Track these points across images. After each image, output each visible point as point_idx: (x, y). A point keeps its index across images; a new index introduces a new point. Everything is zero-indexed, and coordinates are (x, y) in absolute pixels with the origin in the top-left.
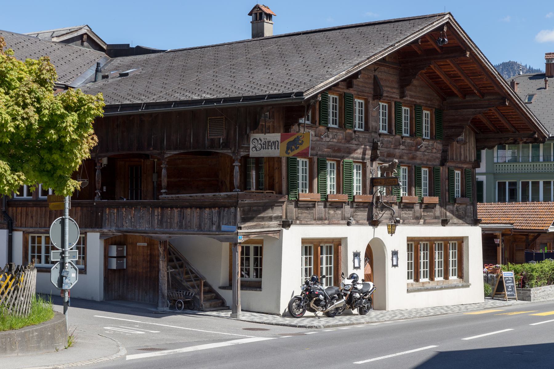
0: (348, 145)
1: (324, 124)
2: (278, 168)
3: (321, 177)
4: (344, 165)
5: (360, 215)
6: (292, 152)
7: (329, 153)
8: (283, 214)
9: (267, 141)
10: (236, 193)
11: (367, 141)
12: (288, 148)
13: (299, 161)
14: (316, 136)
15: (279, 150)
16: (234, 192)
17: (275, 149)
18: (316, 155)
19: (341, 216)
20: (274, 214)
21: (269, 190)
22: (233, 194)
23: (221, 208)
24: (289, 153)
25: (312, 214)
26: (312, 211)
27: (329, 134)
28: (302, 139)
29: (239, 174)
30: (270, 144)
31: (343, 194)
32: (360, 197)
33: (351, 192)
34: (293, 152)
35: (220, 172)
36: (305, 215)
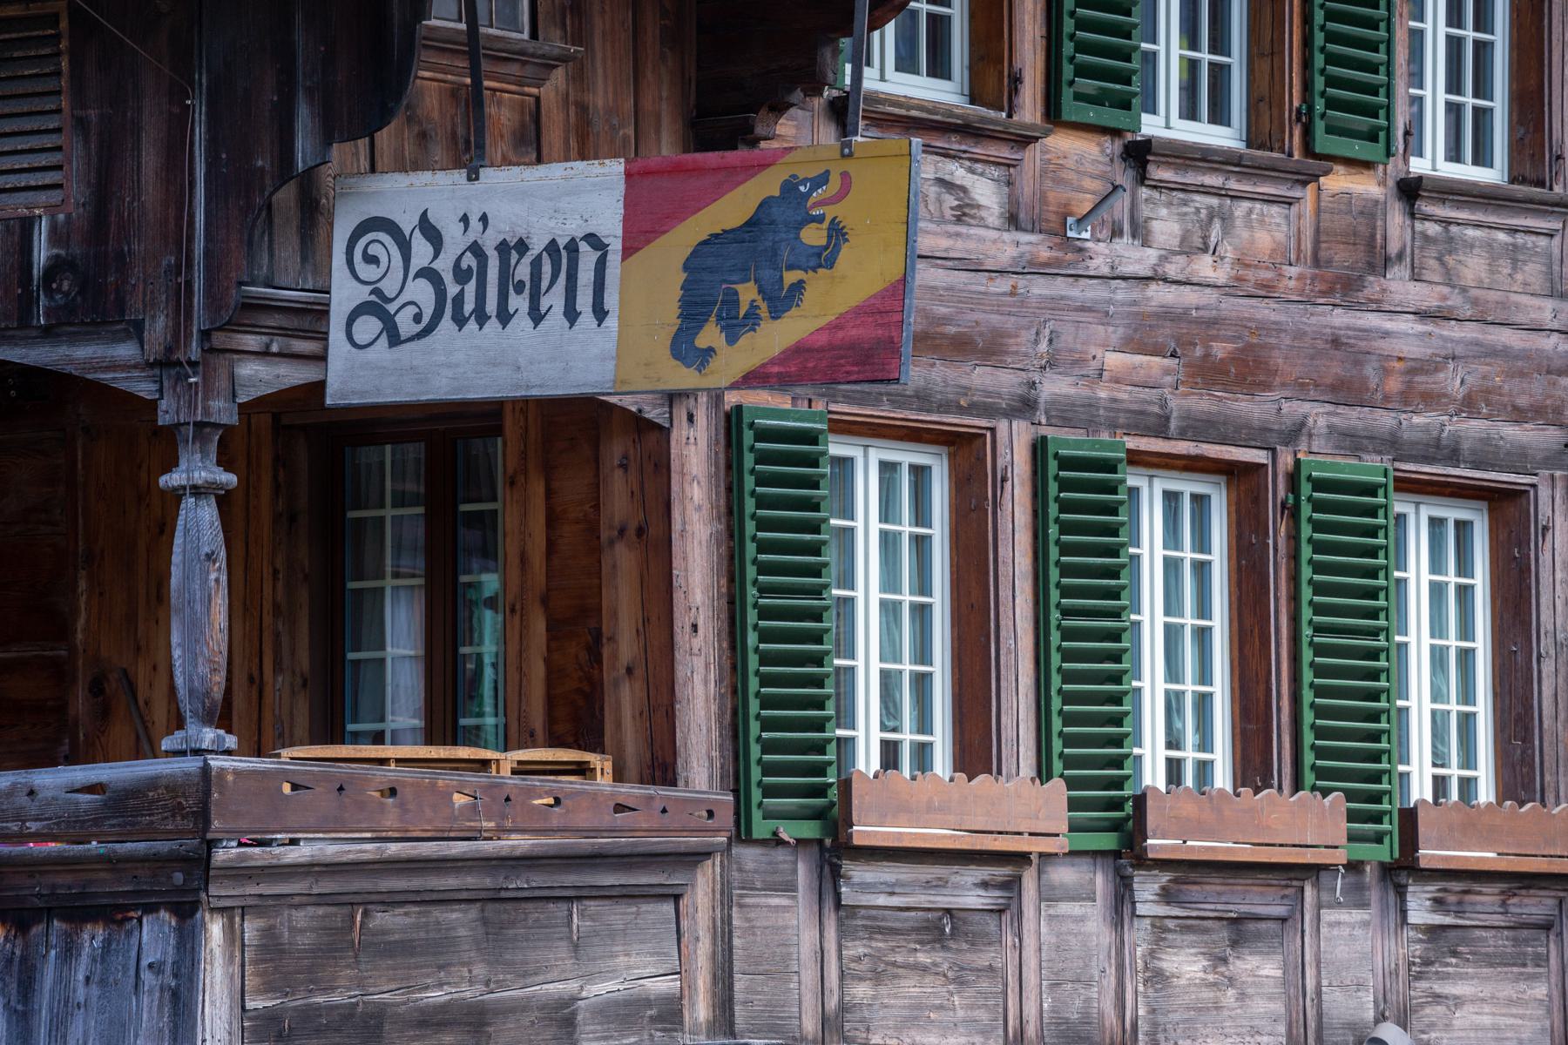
0: (1340, 318)
1: (1091, 114)
2: (640, 532)
3: (1069, 623)
4: (1306, 510)
5: (1475, 1000)
6: (732, 340)
7: (1146, 394)
8: (689, 986)
9: (489, 244)
10: (192, 764)
11: (1538, 283)
12: (694, 311)
13: (845, 464)
14: (1012, 221)
15: (612, 322)
16: (168, 754)
17: (571, 315)
18: (1025, 406)
19: (1278, 1007)
20: (590, 977)
21: (555, 741)
22: (153, 783)
23: (37, 930)
24: (710, 351)
25: (984, 985)
26: (983, 959)
27: (1145, 211)
28: (830, 212)
29: (217, 575)
30: (523, 272)
31: (1297, 786)
32: (1471, 823)
33: (1376, 777)
34: (743, 341)
35: (83, 585)
36: (911, 987)
